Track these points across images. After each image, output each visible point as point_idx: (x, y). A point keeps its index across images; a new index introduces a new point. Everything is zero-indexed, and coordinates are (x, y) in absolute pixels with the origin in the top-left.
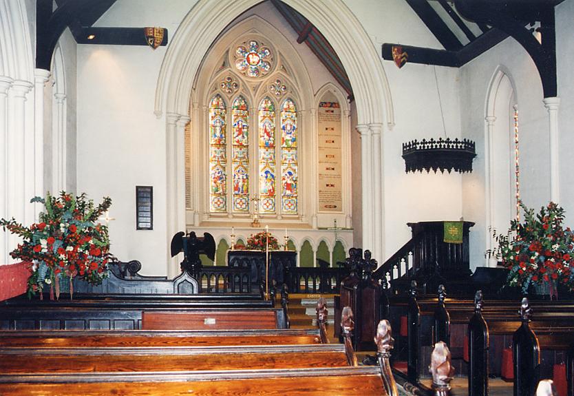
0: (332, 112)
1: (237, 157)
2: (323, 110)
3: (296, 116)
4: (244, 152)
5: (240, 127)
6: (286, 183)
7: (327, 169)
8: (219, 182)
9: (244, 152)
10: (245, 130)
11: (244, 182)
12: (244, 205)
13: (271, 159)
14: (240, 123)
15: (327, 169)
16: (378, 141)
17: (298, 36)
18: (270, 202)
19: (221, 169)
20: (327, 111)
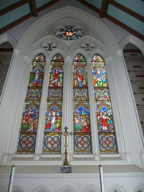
0: (136, 55)
1: (52, 97)
2: (128, 54)
3: (105, 65)
4: (59, 92)
5: (57, 73)
6: (101, 118)
7: (134, 67)
8: (31, 119)
9: (59, 92)
10: (61, 75)
11: (56, 119)
12: (50, 146)
13: (84, 97)
14: (57, 70)
15: (134, 67)
16: (11, 182)
17: (99, 15)
18: (85, 139)
19: (34, 108)
20: (131, 55)
